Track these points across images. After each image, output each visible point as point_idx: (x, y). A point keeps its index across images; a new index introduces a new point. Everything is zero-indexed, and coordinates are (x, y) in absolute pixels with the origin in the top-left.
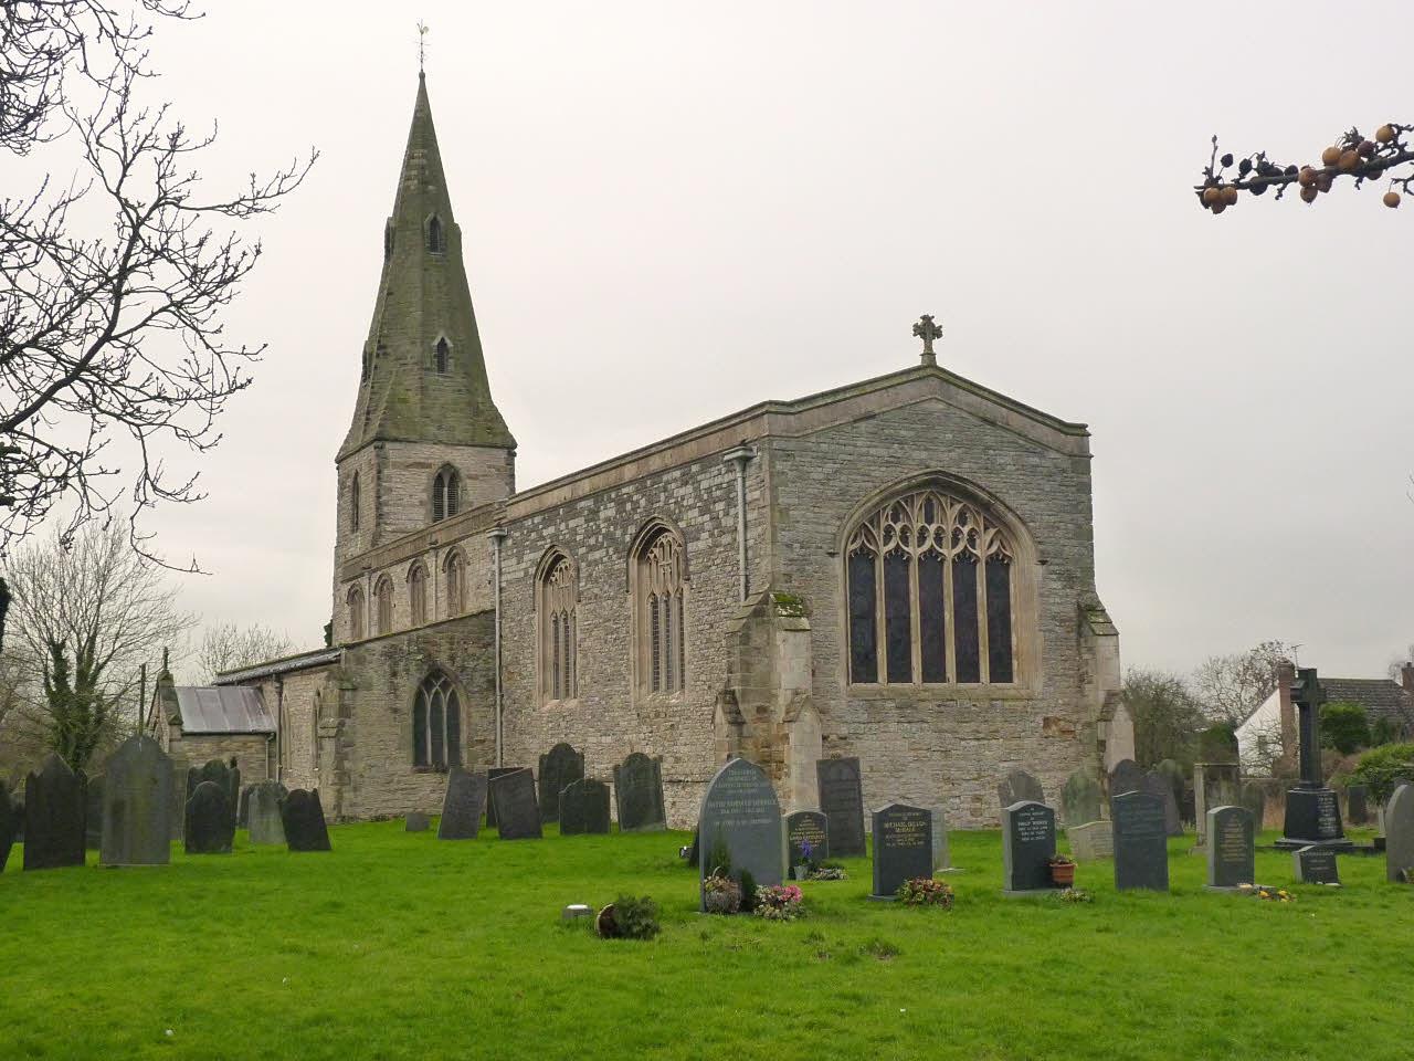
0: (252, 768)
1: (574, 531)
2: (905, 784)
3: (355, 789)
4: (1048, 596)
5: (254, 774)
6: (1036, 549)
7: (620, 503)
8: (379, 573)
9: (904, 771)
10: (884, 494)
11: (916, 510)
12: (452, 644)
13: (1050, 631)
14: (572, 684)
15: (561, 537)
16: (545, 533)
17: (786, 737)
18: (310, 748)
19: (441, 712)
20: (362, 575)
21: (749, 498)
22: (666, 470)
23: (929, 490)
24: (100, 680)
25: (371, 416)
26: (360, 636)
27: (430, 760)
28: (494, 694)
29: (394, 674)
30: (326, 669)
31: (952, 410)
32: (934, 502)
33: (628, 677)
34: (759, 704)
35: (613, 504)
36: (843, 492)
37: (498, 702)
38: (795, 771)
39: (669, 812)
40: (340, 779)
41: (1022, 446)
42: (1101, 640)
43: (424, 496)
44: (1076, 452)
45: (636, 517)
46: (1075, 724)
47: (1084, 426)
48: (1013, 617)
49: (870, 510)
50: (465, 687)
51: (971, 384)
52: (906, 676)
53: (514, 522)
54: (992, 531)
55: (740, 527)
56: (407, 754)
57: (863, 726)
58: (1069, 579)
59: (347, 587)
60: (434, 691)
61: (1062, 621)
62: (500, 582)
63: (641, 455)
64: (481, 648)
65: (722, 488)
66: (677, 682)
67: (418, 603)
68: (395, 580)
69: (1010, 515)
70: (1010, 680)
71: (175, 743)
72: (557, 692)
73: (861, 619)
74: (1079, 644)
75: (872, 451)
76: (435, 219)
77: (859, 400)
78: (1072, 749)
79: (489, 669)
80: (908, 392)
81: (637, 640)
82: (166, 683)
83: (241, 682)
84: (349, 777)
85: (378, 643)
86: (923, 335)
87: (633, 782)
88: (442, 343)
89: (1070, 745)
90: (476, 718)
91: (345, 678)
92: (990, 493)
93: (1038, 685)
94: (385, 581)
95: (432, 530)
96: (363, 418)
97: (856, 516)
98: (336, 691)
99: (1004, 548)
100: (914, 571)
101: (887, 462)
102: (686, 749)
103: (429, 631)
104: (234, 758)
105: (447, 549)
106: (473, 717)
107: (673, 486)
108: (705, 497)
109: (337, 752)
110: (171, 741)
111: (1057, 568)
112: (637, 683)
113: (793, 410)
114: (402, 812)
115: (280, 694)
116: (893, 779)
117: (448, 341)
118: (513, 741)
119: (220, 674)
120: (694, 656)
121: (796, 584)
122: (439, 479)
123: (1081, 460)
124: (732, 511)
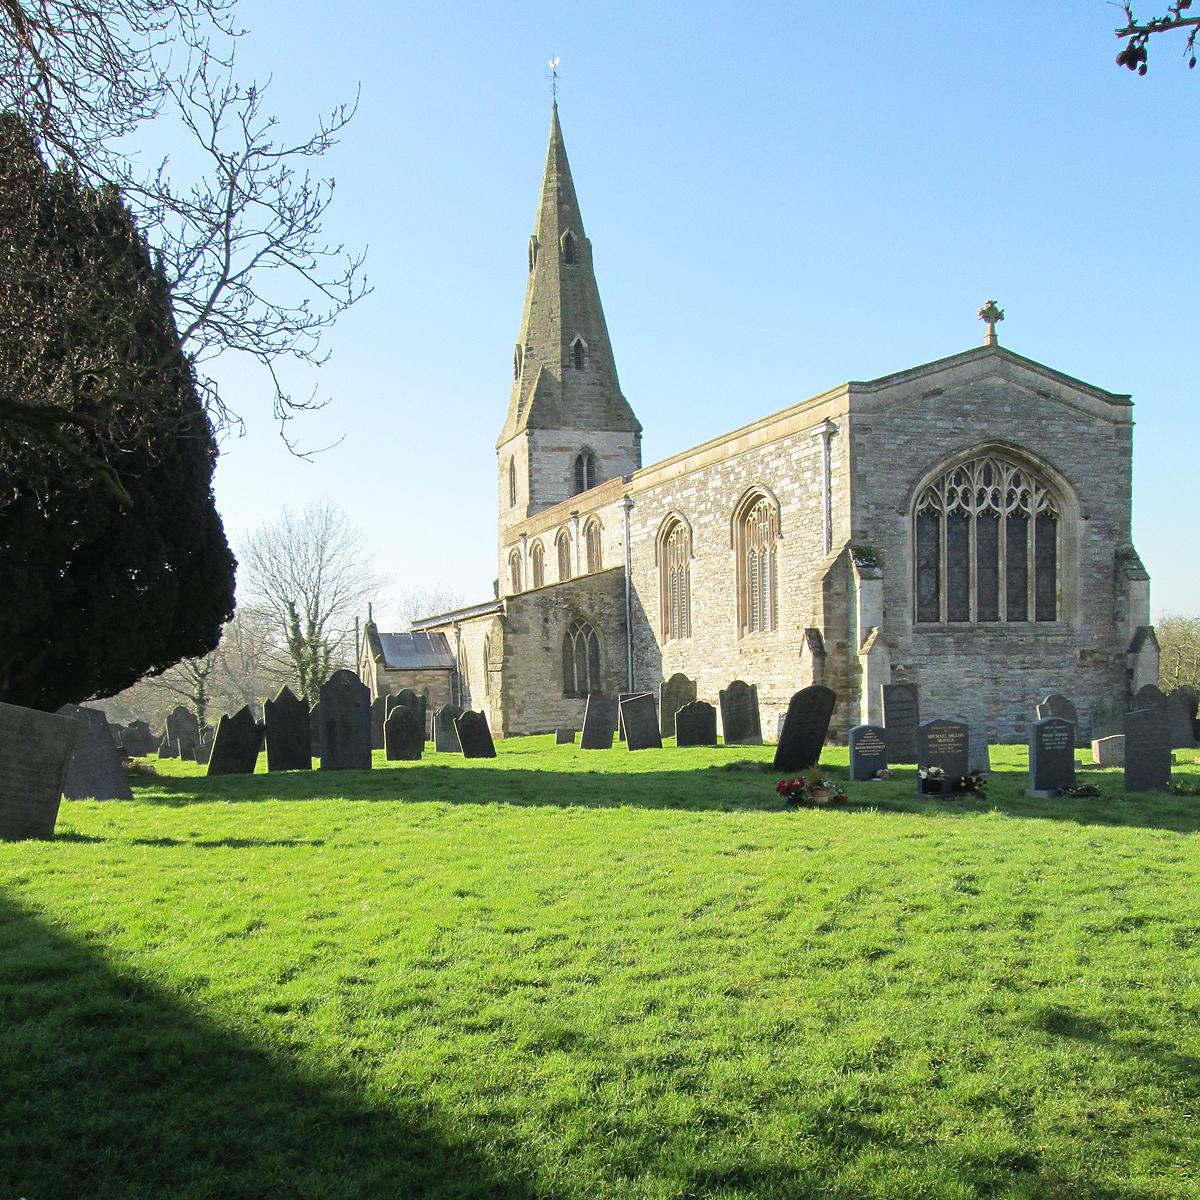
2: (960, 705)
7: (726, 475)
11: (976, 475)
16: (664, 501)
20: (519, 541)
23: (988, 457)
24: (323, 630)
26: (520, 589)
32: (993, 470)
35: (719, 476)
36: (913, 460)
42: (1134, 584)
43: (568, 475)
45: (738, 486)
54: (1043, 492)
58: (1110, 532)
59: (509, 549)
60: (578, 633)
73: (927, 566)
75: (939, 424)
93: (1078, 622)
96: (517, 410)
98: (501, 635)
100: (1031, 526)
101: (952, 433)
102: (780, 677)
108: (795, 467)
117: (583, 341)
119: (415, 623)
121: (871, 540)
122: (579, 460)
123: (1123, 430)
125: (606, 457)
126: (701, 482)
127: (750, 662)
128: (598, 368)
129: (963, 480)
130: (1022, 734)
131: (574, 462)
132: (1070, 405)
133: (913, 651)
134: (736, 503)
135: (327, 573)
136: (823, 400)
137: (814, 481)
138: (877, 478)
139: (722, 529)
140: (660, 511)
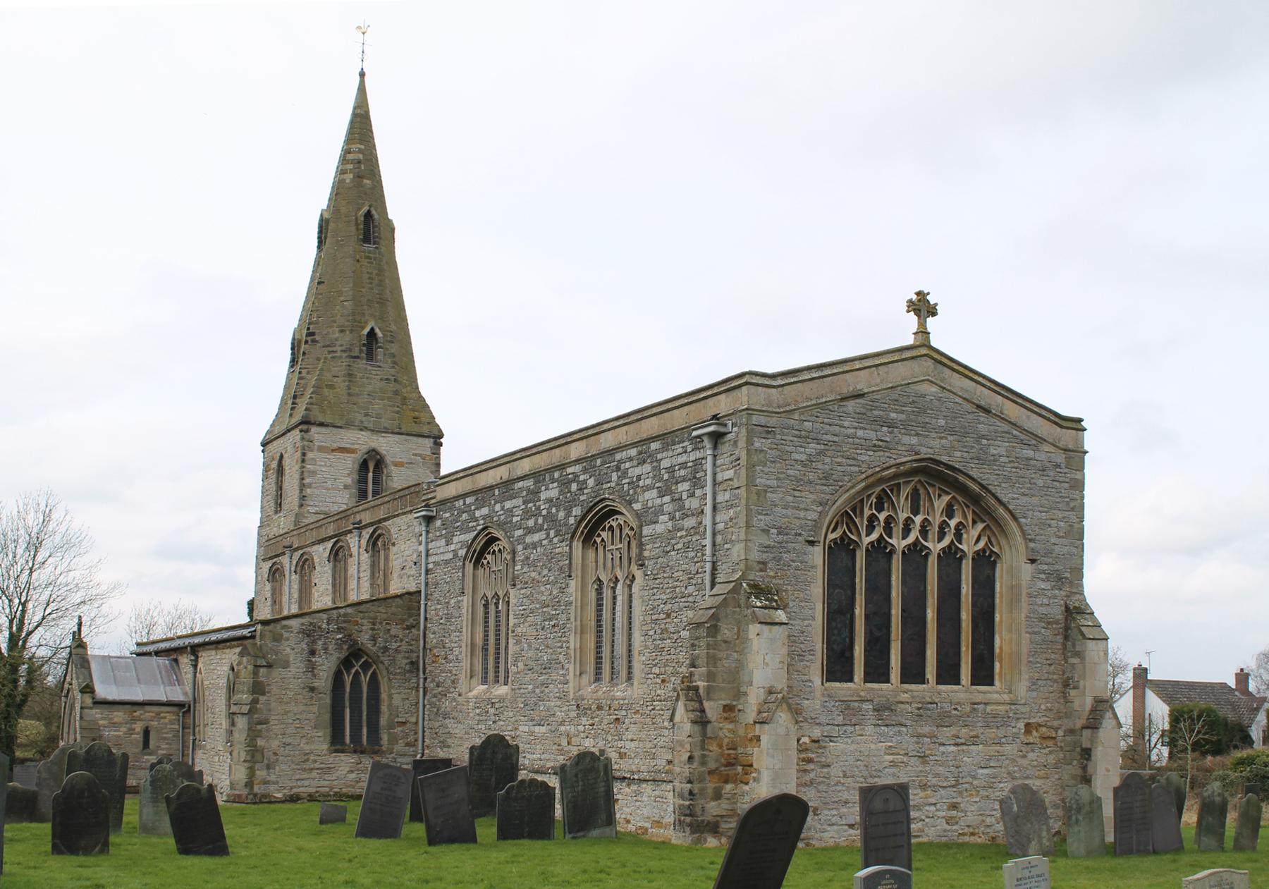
0: (165, 738)
3: (268, 767)
4: (1036, 597)
5: (167, 744)
6: (1027, 547)
7: (565, 483)
8: (300, 552)
9: (879, 777)
10: (871, 479)
11: (902, 500)
13: (1035, 633)
14: (502, 669)
15: (495, 519)
16: (478, 514)
17: (758, 739)
18: (224, 722)
19: (361, 692)
20: (283, 554)
21: (720, 477)
23: (916, 479)
24: (29, 644)
25: (298, 400)
26: (281, 611)
27: (348, 740)
29: (313, 653)
30: (241, 645)
32: (922, 496)
34: (724, 703)
36: (827, 476)
37: (421, 685)
39: (622, 811)
40: (253, 757)
41: (1016, 437)
42: (1091, 644)
43: (349, 481)
44: (1070, 447)
45: (582, 498)
46: (1056, 729)
47: (1080, 420)
48: (997, 618)
49: (853, 497)
50: (387, 669)
51: (966, 367)
52: (921, 679)
53: (443, 502)
54: (980, 526)
55: (708, 509)
57: (837, 728)
58: (1059, 580)
59: (269, 564)
61: (1049, 623)
63: (590, 432)
64: (405, 629)
65: (686, 468)
67: (339, 583)
68: (316, 559)
69: (1001, 510)
70: (991, 683)
71: (86, 711)
72: (486, 678)
73: (839, 615)
75: (860, 433)
76: (369, 211)
78: (1052, 756)
79: (412, 651)
81: (579, 628)
82: (80, 650)
83: (158, 653)
84: (263, 754)
85: (295, 620)
86: (917, 312)
87: (580, 783)
88: (372, 333)
89: (1051, 752)
90: (397, 700)
91: (260, 655)
93: (1022, 689)
95: (356, 510)
96: (290, 402)
97: (838, 504)
98: (250, 667)
99: (992, 545)
100: (897, 564)
101: (875, 446)
102: (633, 745)
103: (349, 610)
104: (147, 728)
105: (371, 530)
106: (394, 698)
107: (628, 465)
108: (666, 477)
109: (249, 729)
110: (82, 708)
111: (1046, 567)
112: (578, 673)
113: (774, 383)
114: (317, 792)
115: (195, 666)
117: (377, 330)
118: (437, 724)
119: (138, 644)
121: (772, 574)
122: (364, 466)
123: (1076, 456)
124: (698, 493)
125: (396, 464)
126: (528, 490)
127: (590, 722)
128: (395, 363)
129: (886, 505)
130: (955, 827)
131: (357, 467)
133: (823, 719)
134: (579, 518)
135: (40, 577)
136: (710, 393)
137: (693, 495)
138: (781, 495)
139: (557, 551)
140: (471, 525)
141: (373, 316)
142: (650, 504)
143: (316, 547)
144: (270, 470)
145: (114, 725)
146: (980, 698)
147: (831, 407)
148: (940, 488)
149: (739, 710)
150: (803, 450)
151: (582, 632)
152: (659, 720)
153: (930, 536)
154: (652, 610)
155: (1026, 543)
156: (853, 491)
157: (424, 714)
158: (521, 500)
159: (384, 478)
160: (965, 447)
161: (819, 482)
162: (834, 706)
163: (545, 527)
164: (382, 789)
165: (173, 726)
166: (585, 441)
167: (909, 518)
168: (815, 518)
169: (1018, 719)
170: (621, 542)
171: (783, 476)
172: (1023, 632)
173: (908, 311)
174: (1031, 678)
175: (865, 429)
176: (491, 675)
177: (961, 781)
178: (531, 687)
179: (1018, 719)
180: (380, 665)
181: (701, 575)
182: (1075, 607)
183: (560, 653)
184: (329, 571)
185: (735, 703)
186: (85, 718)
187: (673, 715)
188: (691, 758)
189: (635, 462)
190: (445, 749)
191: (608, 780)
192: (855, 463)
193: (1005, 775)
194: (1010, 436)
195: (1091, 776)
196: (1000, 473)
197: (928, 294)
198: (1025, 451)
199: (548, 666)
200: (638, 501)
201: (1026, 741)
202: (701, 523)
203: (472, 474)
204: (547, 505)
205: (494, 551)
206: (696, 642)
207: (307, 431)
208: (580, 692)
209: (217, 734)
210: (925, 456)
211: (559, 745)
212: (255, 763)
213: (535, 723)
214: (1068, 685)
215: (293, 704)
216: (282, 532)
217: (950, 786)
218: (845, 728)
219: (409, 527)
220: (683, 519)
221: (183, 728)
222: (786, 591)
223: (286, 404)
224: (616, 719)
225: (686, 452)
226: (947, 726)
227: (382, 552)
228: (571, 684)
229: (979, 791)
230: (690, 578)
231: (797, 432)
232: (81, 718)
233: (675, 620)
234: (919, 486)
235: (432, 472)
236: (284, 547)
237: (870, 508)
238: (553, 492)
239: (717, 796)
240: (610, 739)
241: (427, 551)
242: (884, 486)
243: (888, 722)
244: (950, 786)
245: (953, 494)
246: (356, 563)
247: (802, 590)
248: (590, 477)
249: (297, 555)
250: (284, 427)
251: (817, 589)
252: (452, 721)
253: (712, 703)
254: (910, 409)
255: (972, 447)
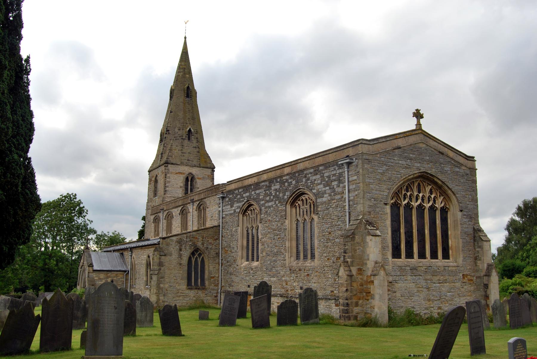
1: (259, 195)
2: (413, 302)
6: (459, 205)
7: (282, 183)
8: (167, 211)
9: (413, 296)
10: (405, 180)
11: (415, 188)
12: (203, 238)
15: (252, 197)
16: (244, 195)
17: (372, 282)
18: (144, 278)
19: (192, 265)
20: (160, 212)
21: (350, 179)
22: (306, 169)
23: (419, 180)
27: (193, 284)
28: (219, 258)
29: (181, 250)
31: (428, 147)
32: (422, 186)
33: (285, 254)
35: (278, 184)
37: (220, 262)
38: (377, 297)
41: (453, 164)
42: (485, 243)
43: (182, 185)
44: (471, 167)
45: (290, 188)
47: (473, 157)
48: (450, 233)
49: (398, 187)
50: (208, 256)
51: (434, 137)
56: (185, 282)
59: (153, 216)
60: (195, 257)
61: (468, 235)
62: (222, 215)
64: (214, 240)
65: (335, 176)
66: (309, 256)
67: (184, 224)
69: (450, 192)
70: (449, 259)
71: (90, 274)
73: (395, 231)
74: (474, 244)
75: (400, 162)
76: (188, 86)
77: (395, 141)
78: (472, 287)
80: (412, 139)
81: (290, 239)
82: (87, 250)
85: (174, 237)
86: (417, 117)
88: (190, 130)
92: (442, 181)
93: (460, 260)
94: (170, 214)
96: (160, 156)
101: (406, 167)
103: (194, 233)
104: (112, 280)
106: (210, 267)
107: (310, 175)
109: (158, 280)
110: (88, 273)
111: (466, 213)
116: (409, 300)
117: (192, 129)
118: (227, 277)
120: (320, 246)
121: (373, 216)
122: (187, 179)
123: (473, 170)
124: (341, 185)
128: (197, 141)
129: (409, 190)
132: (452, 159)
133: (393, 273)
134: (289, 196)
139: (280, 209)
140: (241, 200)
141: (190, 124)
142: (320, 190)
143: (174, 210)
144: (152, 181)
145: (100, 279)
146: (446, 264)
147: (390, 152)
148: (427, 183)
149: (364, 270)
150: (381, 168)
151: (291, 240)
152: (326, 274)
153: (425, 201)
154: (322, 231)
155: (459, 204)
156: (399, 184)
157: (221, 273)
158: (263, 190)
159: (194, 184)
160: (436, 167)
161: (387, 181)
162: (396, 268)
163: (274, 200)
164: (229, 304)
165: (122, 280)
166: (290, 167)
167: (417, 194)
168: (387, 195)
169: (460, 272)
170: (307, 205)
171: (375, 178)
172: (460, 239)
173: (413, 117)
174: (463, 256)
175: (402, 161)
176: (250, 257)
177: (442, 298)
178: (269, 262)
179: (460, 272)
180: (205, 254)
181: (344, 217)
182: (477, 229)
183: (282, 249)
184: (180, 219)
185: (362, 267)
186: (90, 277)
187: (338, 272)
188: (347, 290)
189: (313, 174)
190: (231, 287)
191: (316, 299)
192: (399, 173)
193: (457, 295)
194: (451, 163)
195: (489, 295)
196: (448, 177)
197: (420, 110)
198: (456, 169)
199: (276, 254)
200: (314, 189)
201: (463, 281)
202: (343, 197)
203: (242, 180)
204: (275, 192)
205: (251, 209)
206: (346, 243)
207: (167, 166)
208: (291, 264)
209: (141, 282)
210: (423, 171)
211: (282, 285)
212: (159, 294)
213: (271, 276)
214: (477, 259)
215: (173, 270)
216: (157, 204)
217: (438, 300)
218: (400, 277)
219: (214, 201)
220: (335, 196)
221: (126, 280)
222: (378, 223)
223: (158, 156)
224: (307, 274)
225: (335, 170)
226: (436, 276)
227: (202, 211)
228: (287, 261)
229: (448, 302)
230: (339, 218)
231: (379, 162)
232: (88, 277)
233: (333, 235)
234: (420, 182)
235: (211, 181)
236: (161, 210)
237: (404, 191)
238: (277, 186)
239: (357, 305)
240: (305, 283)
241: (222, 210)
242: (409, 182)
243: (415, 274)
244: (438, 300)
245: (432, 185)
246: (192, 215)
247: (383, 223)
248: (293, 180)
249: (165, 213)
250: (158, 165)
251: (388, 222)
252: (234, 276)
253: (354, 267)
254: (417, 153)
255: (438, 167)
